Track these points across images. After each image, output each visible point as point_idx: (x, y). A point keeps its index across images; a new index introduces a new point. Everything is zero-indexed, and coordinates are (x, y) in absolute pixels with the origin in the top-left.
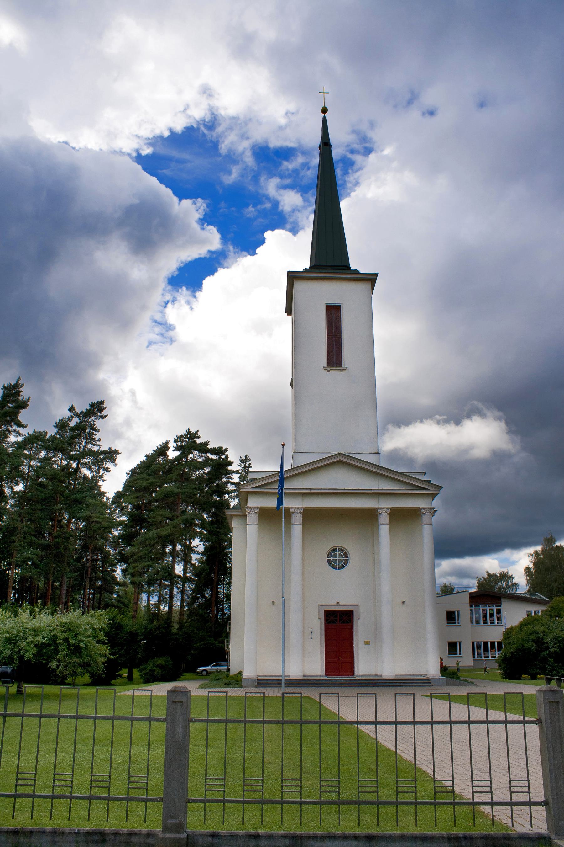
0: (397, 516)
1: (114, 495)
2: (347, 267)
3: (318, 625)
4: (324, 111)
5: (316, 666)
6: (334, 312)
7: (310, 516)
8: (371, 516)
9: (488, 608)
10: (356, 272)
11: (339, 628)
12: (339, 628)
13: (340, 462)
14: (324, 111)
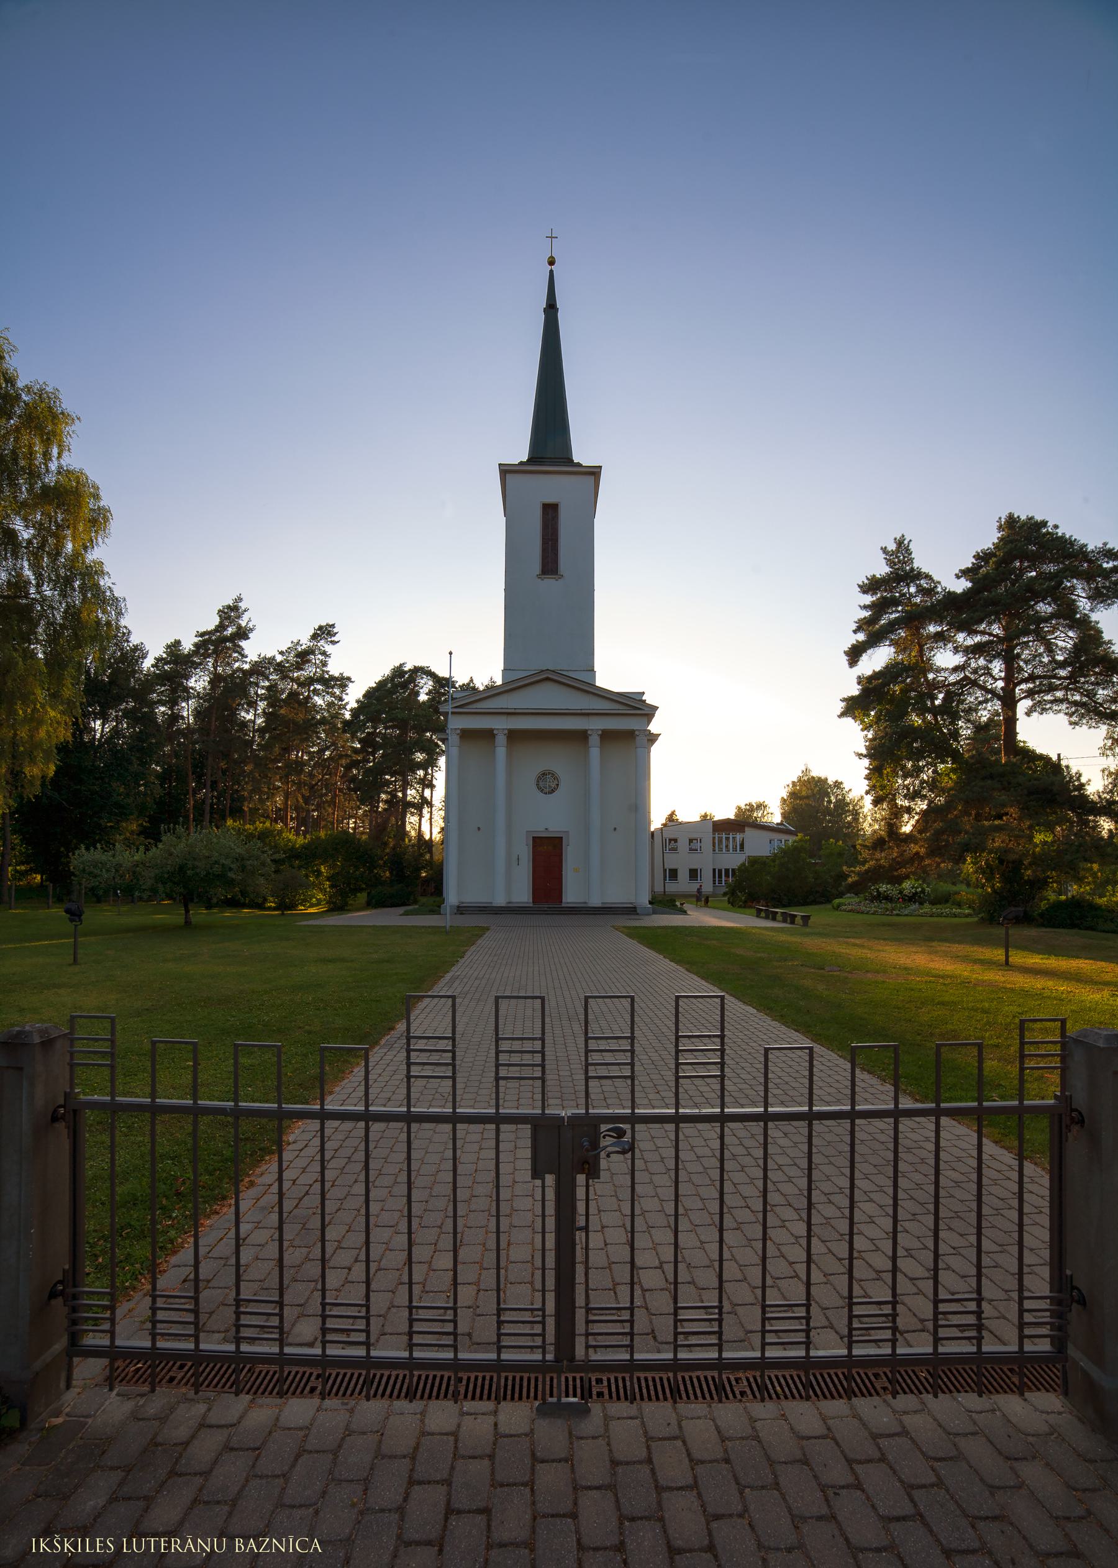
0: (607, 736)
1: (696, 818)
2: (569, 461)
3: (524, 852)
4: (552, 262)
5: (523, 894)
6: (550, 511)
7: (513, 736)
8: (582, 736)
9: (724, 836)
10: (579, 465)
11: (547, 856)
12: (547, 856)
13: (548, 679)
14: (552, 262)
